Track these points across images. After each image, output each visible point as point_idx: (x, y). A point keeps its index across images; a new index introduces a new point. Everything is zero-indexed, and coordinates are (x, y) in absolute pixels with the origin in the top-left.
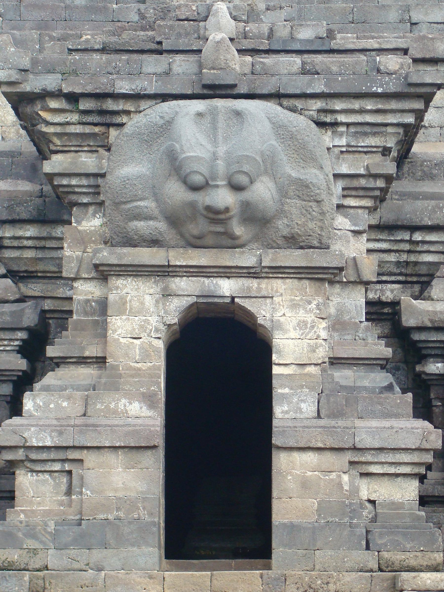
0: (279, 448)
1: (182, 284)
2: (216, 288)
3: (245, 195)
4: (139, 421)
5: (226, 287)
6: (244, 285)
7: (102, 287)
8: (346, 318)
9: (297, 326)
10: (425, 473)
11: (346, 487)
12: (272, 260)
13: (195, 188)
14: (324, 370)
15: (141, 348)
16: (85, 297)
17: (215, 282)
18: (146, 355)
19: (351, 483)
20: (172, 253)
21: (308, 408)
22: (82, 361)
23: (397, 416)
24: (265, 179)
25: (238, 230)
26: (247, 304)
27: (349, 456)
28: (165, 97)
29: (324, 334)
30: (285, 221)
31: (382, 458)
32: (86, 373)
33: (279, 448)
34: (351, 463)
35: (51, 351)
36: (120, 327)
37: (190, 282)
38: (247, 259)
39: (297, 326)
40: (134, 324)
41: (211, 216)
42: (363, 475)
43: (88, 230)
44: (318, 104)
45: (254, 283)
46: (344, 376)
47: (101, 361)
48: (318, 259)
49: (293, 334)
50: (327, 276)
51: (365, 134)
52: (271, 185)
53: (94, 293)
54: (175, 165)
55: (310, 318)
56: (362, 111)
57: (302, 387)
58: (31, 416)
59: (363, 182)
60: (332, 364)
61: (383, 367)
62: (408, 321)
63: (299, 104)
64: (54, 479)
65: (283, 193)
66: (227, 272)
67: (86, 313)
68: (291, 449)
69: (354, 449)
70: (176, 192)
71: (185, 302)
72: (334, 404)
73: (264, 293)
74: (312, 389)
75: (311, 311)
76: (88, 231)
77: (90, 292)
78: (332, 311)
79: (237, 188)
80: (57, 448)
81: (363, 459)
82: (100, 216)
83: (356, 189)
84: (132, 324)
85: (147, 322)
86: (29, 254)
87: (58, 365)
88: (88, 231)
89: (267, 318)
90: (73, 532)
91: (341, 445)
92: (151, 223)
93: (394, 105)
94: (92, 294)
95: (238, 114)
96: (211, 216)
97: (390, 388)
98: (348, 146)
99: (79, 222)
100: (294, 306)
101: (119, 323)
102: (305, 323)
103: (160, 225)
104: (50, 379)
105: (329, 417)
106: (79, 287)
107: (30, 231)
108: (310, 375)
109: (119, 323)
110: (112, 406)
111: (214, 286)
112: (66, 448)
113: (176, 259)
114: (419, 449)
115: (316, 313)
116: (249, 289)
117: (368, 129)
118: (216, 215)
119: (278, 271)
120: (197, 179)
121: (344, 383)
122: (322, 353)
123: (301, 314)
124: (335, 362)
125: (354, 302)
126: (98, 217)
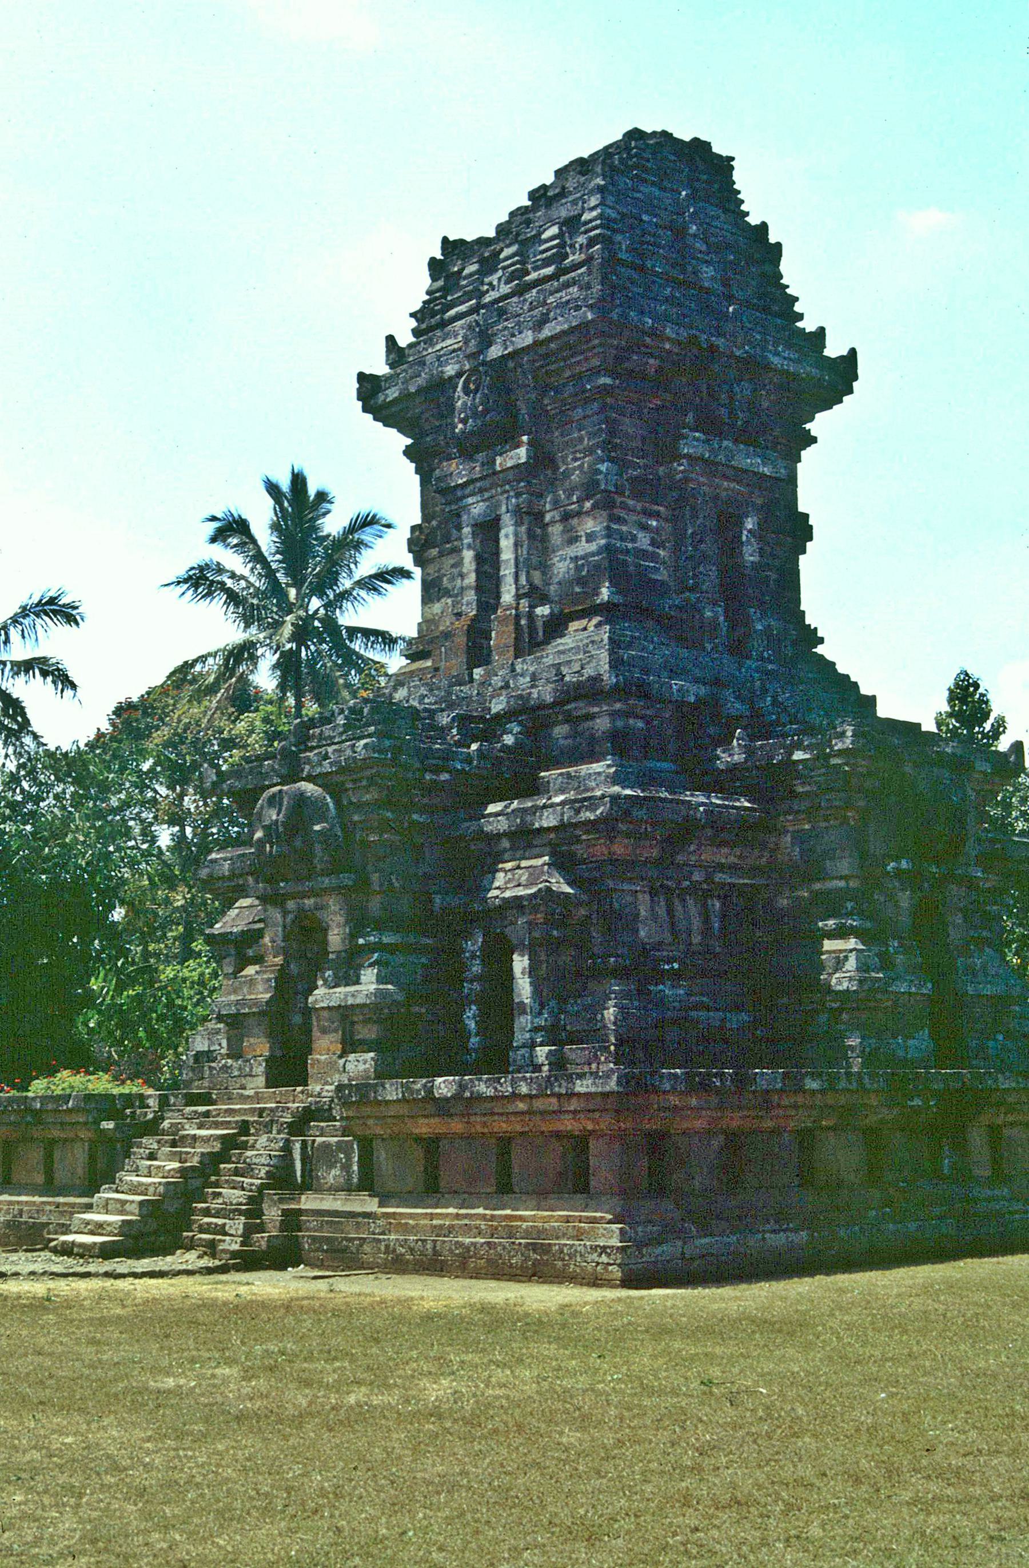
66: (312, 893)
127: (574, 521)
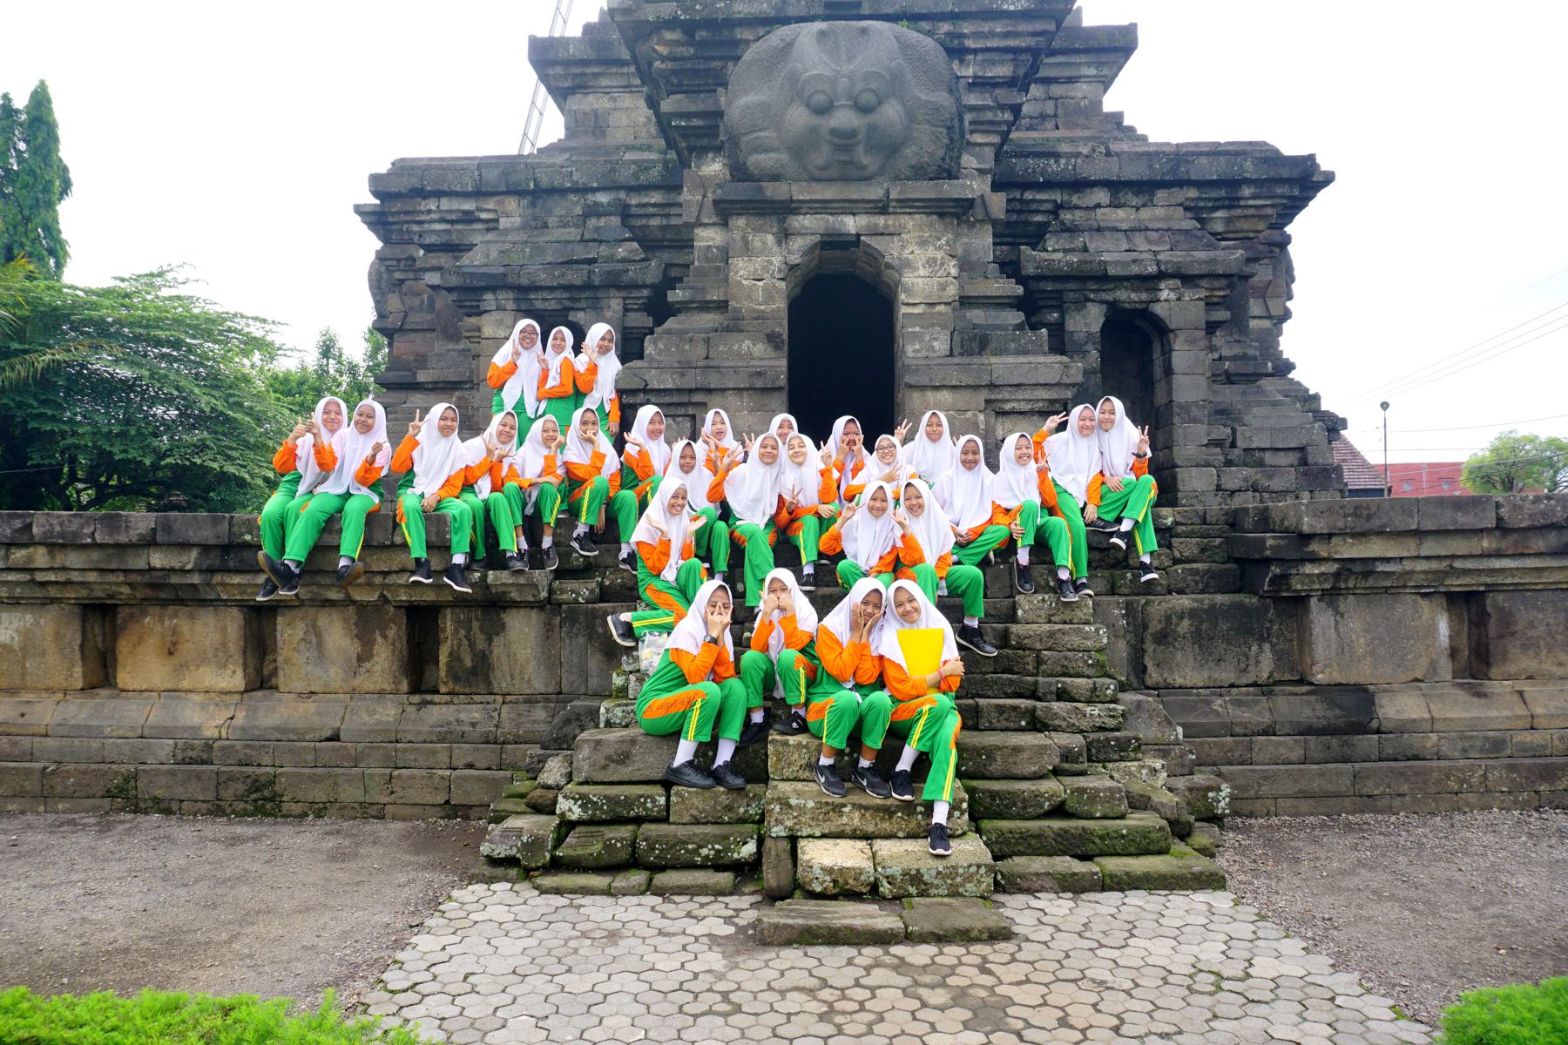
0: (911, 387)
1: (809, 224)
3: (873, 118)
4: (765, 363)
5: (851, 224)
8: (974, 258)
11: (982, 427)
12: (901, 192)
13: (823, 110)
14: (954, 309)
15: (765, 289)
18: (769, 296)
19: (987, 422)
20: (794, 187)
21: (941, 345)
22: (705, 306)
23: (1036, 353)
24: (893, 101)
25: (865, 159)
26: (875, 242)
27: (984, 394)
28: (786, 21)
29: (954, 272)
30: (914, 148)
31: (1020, 395)
32: (708, 320)
33: (911, 387)
34: (988, 402)
35: (677, 295)
36: (742, 269)
38: (875, 192)
41: (837, 141)
42: (997, 413)
44: (945, 27)
45: (881, 221)
46: (977, 316)
47: (722, 306)
48: (950, 189)
49: (922, 272)
50: (958, 212)
51: (993, 63)
52: (899, 107)
54: (796, 90)
55: (939, 255)
56: (992, 34)
57: (933, 325)
58: (652, 360)
59: (989, 115)
60: (962, 304)
61: (1011, 306)
62: (1030, 270)
63: (925, 25)
64: (677, 424)
65: (911, 116)
66: (852, 207)
67: (707, 260)
68: (923, 388)
69: (992, 386)
70: (798, 117)
71: (810, 240)
72: (974, 343)
73: (892, 230)
74: (943, 327)
75: (940, 248)
78: (960, 252)
79: (865, 110)
80: (678, 390)
81: (1000, 397)
83: (983, 123)
85: (770, 262)
86: (655, 222)
87: (679, 311)
91: (978, 382)
92: (773, 155)
93: (1023, 27)
95: (864, 31)
96: (837, 141)
97: (1019, 327)
98: (975, 77)
99: (698, 167)
100: (923, 243)
101: (741, 264)
102: (935, 260)
103: (784, 157)
104: (671, 323)
105: (961, 354)
107: (656, 197)
108: (940, 314)
109: (741, 264)
110: (735, 347)
112: (690, 391)
113: (800, 193)
114: (1058, 384)
117: (996, 56)
118: (844, 140)
119: (908, 206)
120: (820, 99)
121: (975, 321)
122: (952, 291)
123: (931, 252)
124: (965, 302)
125: (982, 242)
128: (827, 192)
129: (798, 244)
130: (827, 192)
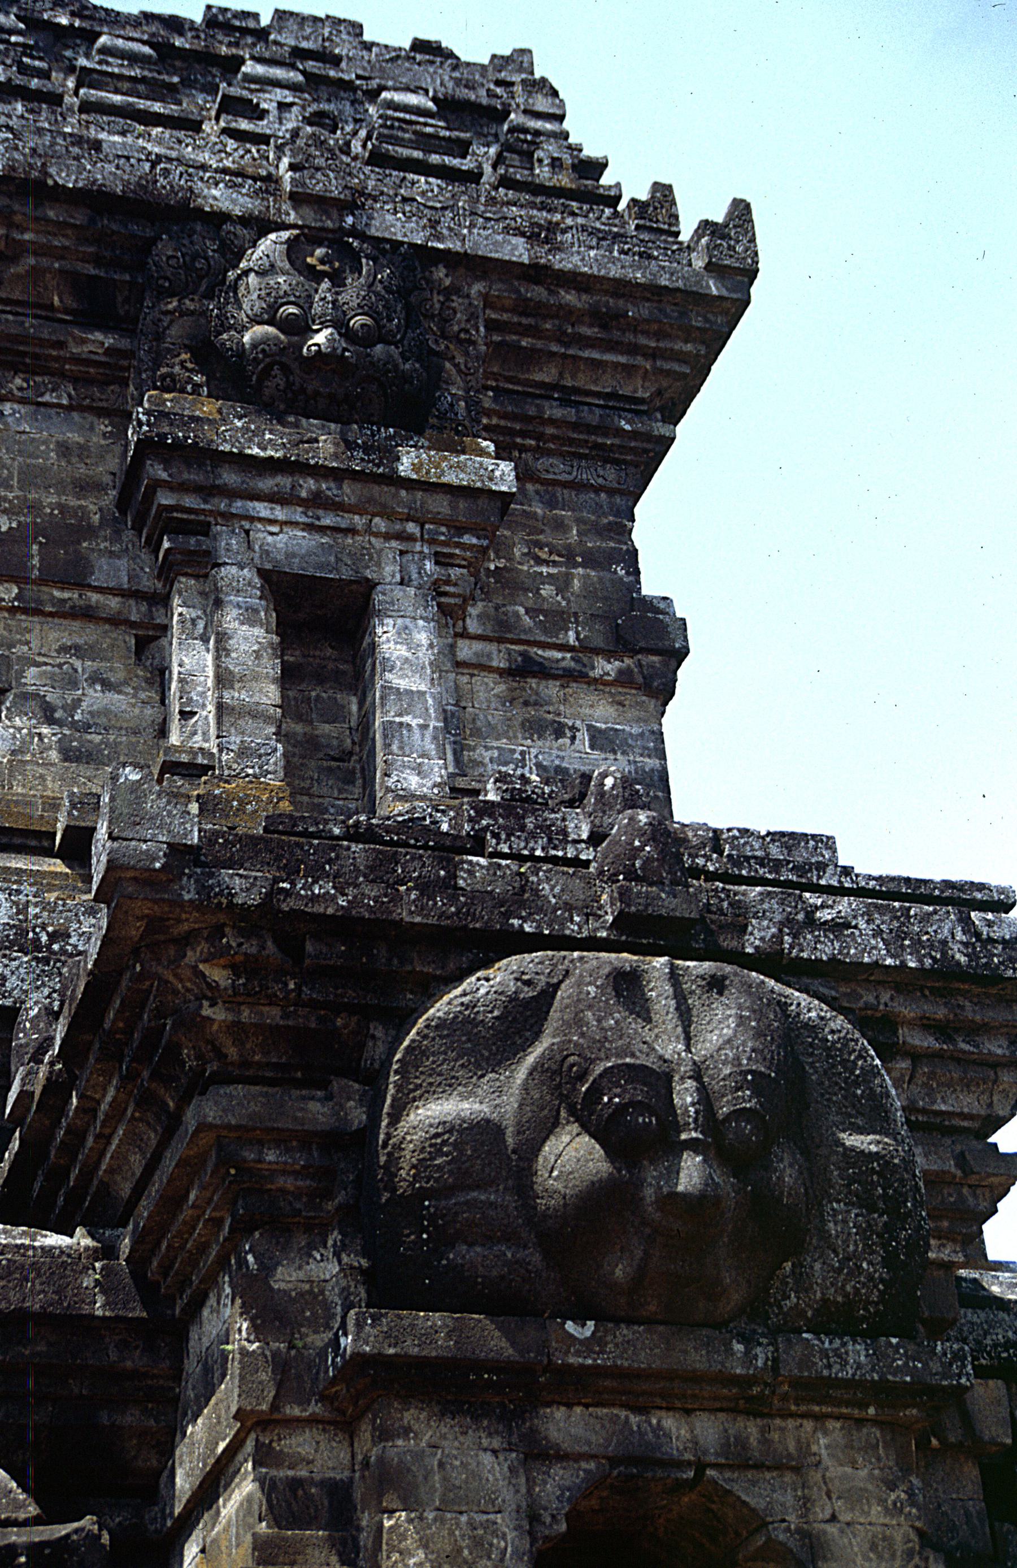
1: (565, 1424)
2: (658, 1437)
6: (726, 1431)
7: (334, 1444)
9: (871, 1549)
10: (96, 1532)
16: (290, 1473)
17: (654, 1421)
37: (592, 1420)
39: (871, 1549)
40: (457, 1533)
43: (291, 1290)
53: (312, 1462)
76: (293, 1294)
77: (303, 1460)
82: (322, 1255)
84: (451, 1533)
88: (293, 1294)
89: (793, 1527)
90: (447, 347)
94: (308, 1463)
106: (274, 1445)
111: (654, 1431)
115: (910, 1513)
116: (742, 1442)
126: (319, 1257)
127: (551, 689)
128: (635, 1348)
129: (556, 1484)
130: (635, 1348)
